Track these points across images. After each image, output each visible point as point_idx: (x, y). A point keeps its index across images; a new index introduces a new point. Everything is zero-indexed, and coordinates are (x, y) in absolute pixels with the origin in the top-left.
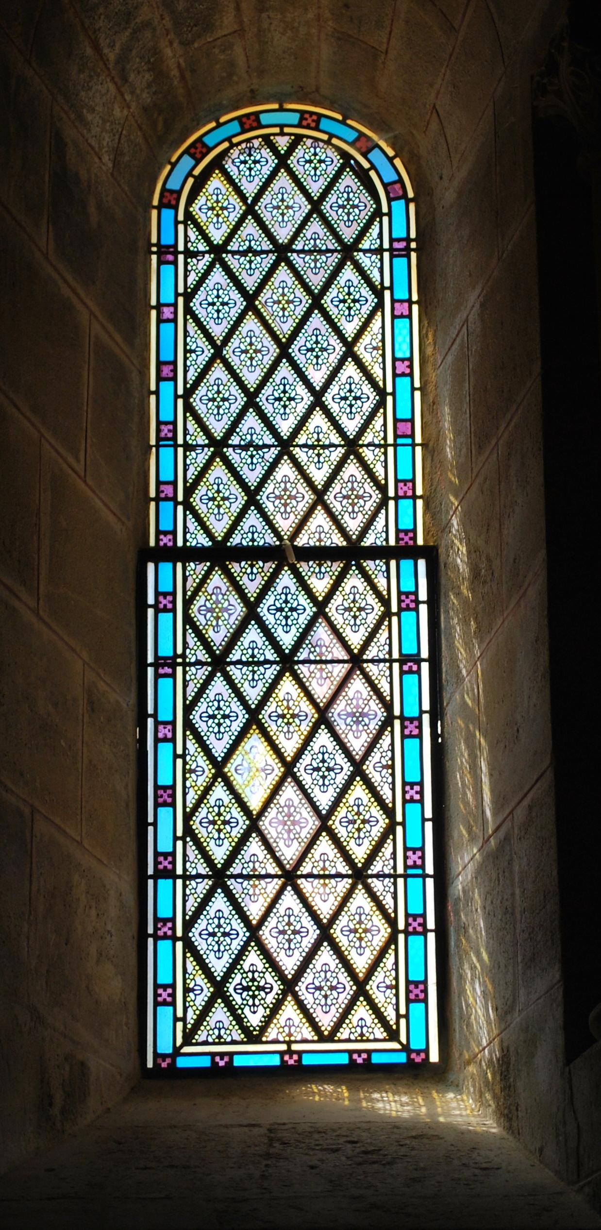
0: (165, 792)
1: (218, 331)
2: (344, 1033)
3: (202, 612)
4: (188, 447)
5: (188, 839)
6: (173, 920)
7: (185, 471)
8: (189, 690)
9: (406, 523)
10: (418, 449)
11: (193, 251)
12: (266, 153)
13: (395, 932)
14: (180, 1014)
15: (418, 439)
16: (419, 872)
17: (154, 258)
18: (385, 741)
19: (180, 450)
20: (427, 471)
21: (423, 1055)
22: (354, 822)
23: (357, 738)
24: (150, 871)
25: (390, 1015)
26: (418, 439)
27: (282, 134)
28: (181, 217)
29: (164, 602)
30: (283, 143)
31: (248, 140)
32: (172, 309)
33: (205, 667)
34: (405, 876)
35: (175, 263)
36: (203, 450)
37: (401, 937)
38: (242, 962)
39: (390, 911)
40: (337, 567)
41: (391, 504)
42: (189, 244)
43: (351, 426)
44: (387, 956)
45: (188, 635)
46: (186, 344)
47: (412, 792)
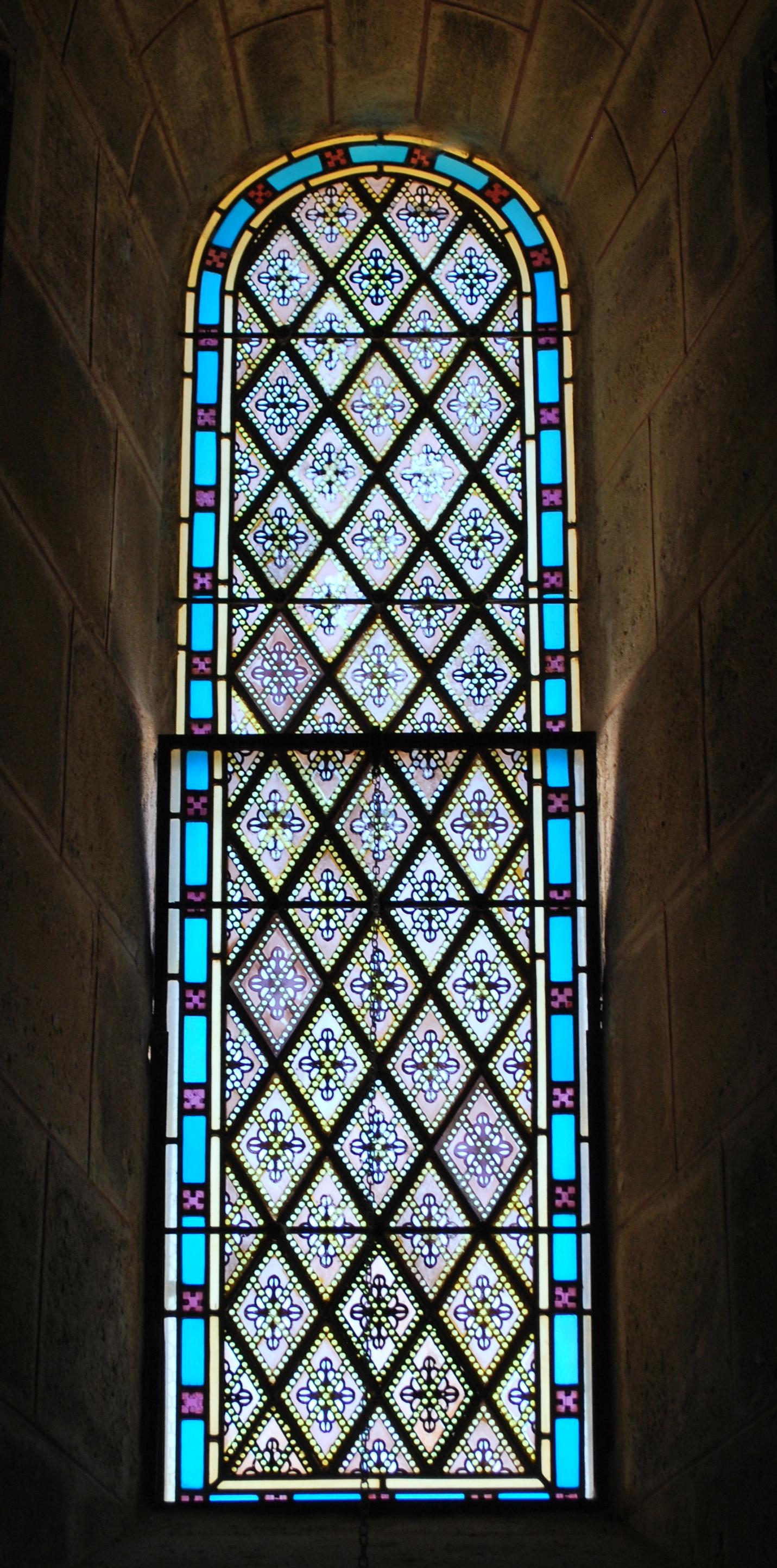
0: (196, 1005)
1: (282, 444)
2: (456, 1462)
3: (251, 1316)
4: (234, 602)
5: (240, 294)
6: (205, 1288)
7: (230, 635)
8: (240, 372)
9: (556, 707)
10: (573, 608)
11: (241, 599)
12: (353, 202)
13: (534, 1313)
14: (214, 1430)
15: (574, 594)
16: (561, 596)
17: (189, 343)
18: (522, 1027)
19: (223, 609)
20: (584, 568)
21: (562, 724)
22: (469, 539)
23: (484, 1349)
24: (183, 593)
25: (527, 1438)
26: (574, 594)
27: (377, 175)
28: (230, 286)
29: (201, 581)
30: (377, 188)
31: (329, 185)
32: (201, 1093)
33: (254, 910)
34: (551, 1230)
35: (220, 349)
36: (260, 342)
37: (544, 1321)
38: (311, 1026)
39: (530, 1450)
40: (454, 757)
41: (535, 686)
42: (240, 325)
43: (477, 579)
44: (519, 1021)
45: (229, 1019)
46: (224, 1053)
47: (562, 998)
